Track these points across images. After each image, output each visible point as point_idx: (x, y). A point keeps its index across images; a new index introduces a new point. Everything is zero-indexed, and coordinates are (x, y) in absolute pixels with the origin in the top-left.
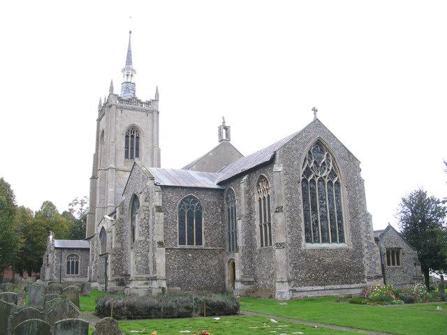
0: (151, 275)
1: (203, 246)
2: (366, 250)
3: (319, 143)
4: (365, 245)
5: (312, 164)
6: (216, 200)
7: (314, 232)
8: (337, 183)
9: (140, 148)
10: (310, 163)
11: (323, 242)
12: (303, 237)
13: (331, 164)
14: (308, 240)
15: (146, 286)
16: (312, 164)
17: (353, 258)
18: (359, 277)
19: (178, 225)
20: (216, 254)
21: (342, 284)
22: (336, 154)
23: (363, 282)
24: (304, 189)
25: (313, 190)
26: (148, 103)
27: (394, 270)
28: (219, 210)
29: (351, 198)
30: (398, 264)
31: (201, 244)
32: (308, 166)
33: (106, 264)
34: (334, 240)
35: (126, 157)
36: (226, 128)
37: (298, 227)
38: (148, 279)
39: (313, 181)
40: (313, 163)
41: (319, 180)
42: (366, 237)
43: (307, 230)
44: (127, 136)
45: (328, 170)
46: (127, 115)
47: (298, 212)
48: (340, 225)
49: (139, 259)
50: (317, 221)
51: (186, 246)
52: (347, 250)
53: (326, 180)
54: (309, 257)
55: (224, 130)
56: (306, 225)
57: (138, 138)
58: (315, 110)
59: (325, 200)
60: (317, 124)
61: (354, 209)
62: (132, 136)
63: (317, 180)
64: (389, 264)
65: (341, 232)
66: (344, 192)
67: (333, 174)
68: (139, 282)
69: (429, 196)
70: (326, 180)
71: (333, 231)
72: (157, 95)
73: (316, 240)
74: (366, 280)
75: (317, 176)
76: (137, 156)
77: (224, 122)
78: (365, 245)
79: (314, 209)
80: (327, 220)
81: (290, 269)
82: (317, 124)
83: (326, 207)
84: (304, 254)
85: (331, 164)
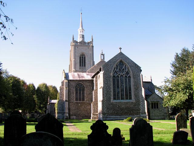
0: (64, 112)
2: (141, 103)
3: (121, 61)
4: (141, 100)
6: (90, 84)
7: (118, 95)
8: (130, 77)
9: (86, 62)
10: (117, 69)
12: (112, 98)
13: (127, 69)
14: (114, 99)
17: (135, 105)
18: (137, 113)
19: (75, 94)
21: (129, 115)
22: (128, 66)
23: (139, 115)
24: (113, 79)
25: (118, 81)
26: (89, 43)
27: (154, 111)
28: (92, 88)
29: (135, 82)
30: (157, 108)
31: (84, 101)
33: (69, 109)
34: (127, 99)
35: (80, 66)
37: (110, 94)
38: (63, 113)
39: (118, 76)
40: (118, 70)
41: (121, 76)
43: (114, 95)
44: (80, 57)
45: (125, 72)
46: (80, 49)
47: (110, 88)
48: (130, 93)
50: (119, 92)
51: (78, 101)
52: (132, 103)
53: (124, 76)
54: (115, 105)
55: (102, 56)
57: (85, 58)
58: (120, 49)
59: (123, 83)
60: (121, 54)
61: (136, 86)
62: (82, 57)
63: (119, 76)
64: (152, 108)
65: (130, 95)
66: (132, 79)
67: (127, 73)
68: (60, 114)
69: (48, 85)
70: (124, 76)
72: (92, 40)
73: (118, 99)
74: (141, 114)
75: (120, 74)
76: (85, 66)
77: (102, 53)
78: (141, 100)
79: (118, 87)
80: (124, 91)
82: (121, 54)
84: (112, 104)
85: (127, 69)
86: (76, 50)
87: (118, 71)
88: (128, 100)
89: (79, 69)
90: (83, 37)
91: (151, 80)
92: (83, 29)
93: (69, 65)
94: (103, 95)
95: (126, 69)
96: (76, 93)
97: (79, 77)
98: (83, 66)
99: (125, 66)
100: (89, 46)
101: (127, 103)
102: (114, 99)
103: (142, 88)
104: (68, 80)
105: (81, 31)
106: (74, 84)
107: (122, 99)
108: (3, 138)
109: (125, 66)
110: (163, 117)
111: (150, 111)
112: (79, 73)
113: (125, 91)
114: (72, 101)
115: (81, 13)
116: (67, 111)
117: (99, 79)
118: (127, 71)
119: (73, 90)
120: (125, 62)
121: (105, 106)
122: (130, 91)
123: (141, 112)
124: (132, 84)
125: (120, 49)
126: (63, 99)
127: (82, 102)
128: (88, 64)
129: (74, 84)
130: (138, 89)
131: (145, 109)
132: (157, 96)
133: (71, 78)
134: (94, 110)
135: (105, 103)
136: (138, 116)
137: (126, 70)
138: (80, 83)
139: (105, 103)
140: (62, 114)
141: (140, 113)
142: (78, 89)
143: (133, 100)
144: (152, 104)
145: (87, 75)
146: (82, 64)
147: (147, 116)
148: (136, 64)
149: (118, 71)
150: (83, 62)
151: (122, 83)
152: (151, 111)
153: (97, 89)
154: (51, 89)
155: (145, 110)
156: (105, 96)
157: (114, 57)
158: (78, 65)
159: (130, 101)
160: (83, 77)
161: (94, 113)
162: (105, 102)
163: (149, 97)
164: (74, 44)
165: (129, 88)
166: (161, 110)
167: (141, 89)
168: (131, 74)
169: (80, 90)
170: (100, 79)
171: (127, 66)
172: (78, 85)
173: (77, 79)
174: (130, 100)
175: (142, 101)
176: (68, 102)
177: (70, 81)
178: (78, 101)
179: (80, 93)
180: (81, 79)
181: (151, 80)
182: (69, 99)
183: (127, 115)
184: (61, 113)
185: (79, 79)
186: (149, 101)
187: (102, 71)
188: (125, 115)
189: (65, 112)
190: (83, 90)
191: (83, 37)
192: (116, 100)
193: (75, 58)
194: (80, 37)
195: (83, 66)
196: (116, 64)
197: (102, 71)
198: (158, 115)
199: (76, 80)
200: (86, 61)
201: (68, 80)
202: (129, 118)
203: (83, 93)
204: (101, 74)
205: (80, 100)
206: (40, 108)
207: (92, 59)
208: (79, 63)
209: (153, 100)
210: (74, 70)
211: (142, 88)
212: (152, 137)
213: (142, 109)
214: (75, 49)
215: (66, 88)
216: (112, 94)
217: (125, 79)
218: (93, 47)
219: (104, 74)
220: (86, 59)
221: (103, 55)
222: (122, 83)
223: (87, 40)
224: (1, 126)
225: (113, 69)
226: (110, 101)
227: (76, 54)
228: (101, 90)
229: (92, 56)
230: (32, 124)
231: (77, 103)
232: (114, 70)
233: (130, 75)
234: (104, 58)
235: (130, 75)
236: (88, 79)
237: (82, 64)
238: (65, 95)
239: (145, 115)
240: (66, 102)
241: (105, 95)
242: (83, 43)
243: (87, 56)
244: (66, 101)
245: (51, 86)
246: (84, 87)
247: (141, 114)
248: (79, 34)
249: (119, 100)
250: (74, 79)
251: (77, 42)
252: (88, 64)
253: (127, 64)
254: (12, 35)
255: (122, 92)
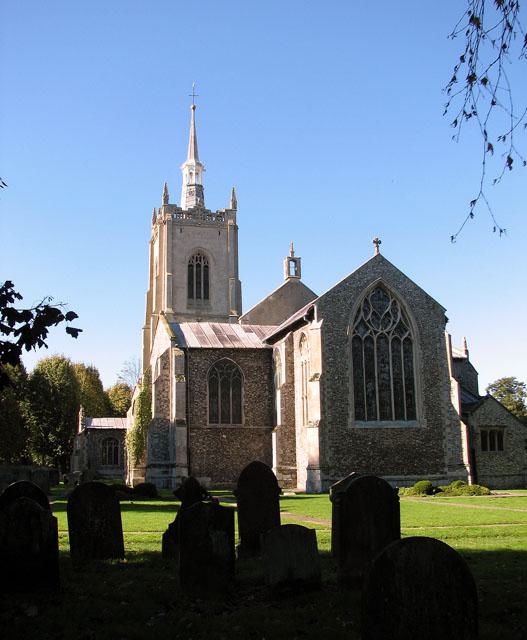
0: (171, 462)
1: (242, 425)
2: (448, 430)
3: (380, 287)
5: (370, 316)
6: (260, 363)
7: (369, 405)
8: (408, 341)
10: (366, 314)
11: (382, 419)
12: (351, 413)
13: (399, 314)
14: (359, 417)
15: (166, 475)
16: (370, 316)
19: (208, 397)
20: (260, 435)
21: (408, 474)
23: (442, 473)
24: (354, 349)
25: (370, 359)
26: (220, 215)
27: (491, 458)
28: (266, 377)
29: (427, 360)
30: (501, 448)
32: (362, 320)
34: (399, 417)
35: (190, 296)
36: (294, 260)
37: (344, 401)
38: (167, 466)
40: (370, 316)
42: (448, 411)
43: (358, 404)
44: (190, 266)
45: (394, 323)
48: (411, 397)
49: (156, 441)
50: (374, 392)
51: (219, 425)
52: (418, 430)
54: (359, 438)
55: (292, 264)
56: (356, 396)
57: (206, 267)
58: (377, 242)
59: (388, 363)
60: (379, 260)
62: (199, 266)
64: (484, 448)
65: (412, 405)
66: (416, 350)
68: (157, 470)
71: (398, 404)
73: (372, 416)
75: (376, 332)
76: (207, 297)
77: (293, 253)
78: (447, 422)
79: (370, 375)
81: (330, 454)
82: (379, 260)
83: (389, 373)
84: (352, 434)
85: (399, 314)
86: (176, 241)
87: (369, 321)
88: (403, 422)
89: (188, 308)
90: (199, 191)
91: (467, 352)
92: (200, 165)
93: (150, 294)
94: (323, 402)
95: (395, 314)
96: (213, 395)
97: (222, 339)
98: (199, 297)
99: (394, 303)
100: (224, 226)
101: (401, 431)
102: (359, 417)
103: (451, 378)
104: (185, 349)
105: (194, 172)
106: (204, 364)
107: (384, 417)
108: (68, 556)
109: (394, 303)
110: (518, 480)
111: (477, 459)
112: (216, 324)
113: (395, 389)
114: (197, 424)
115: (194, 108)
116: (182, 459)
117: (300, 346)
118: (400, 322)
119: (203, 386)
120: (393, 291)
121: (329, 443)
122: (411, 392)
123: (447, 462)
124: (417, 364)
125: (377, 242)
126: (168, 418)
127: (230, 426)
128: (220, 289)
129: (204, 364)
130: (438, 385)
131: (461, 450)
132: (498, 407)
133: (193, 342)
134: (281, 456)
135: (327, 430)
136: (438, 475)
137: (396, 317)
138: (226, 361)
139: (327, 430)
140: (165, 470)
141: (444, 465)
142: (220, 380)
143: (421, 421)
144: (484, 434)
145: (248, 331)
146: (199, 287)
147: (470, 478)
148: (429, 299)
149: (369, 321)
150: (199, 283)
151: (384, 362)
152: (481, 457)
153: (293, 382)
154: (82, 379)
155: (461, 456)
156: (326, 408)
157: (358, 271)
158: (183, 293)
159: (404, 424)
160: (233, 338)
161: (283, 467)
162: (330, 427)
163: (472, 412)
164: (169, 217)
165: (406, 379)
166: (511, 454)
167: (449, 382)
168: (413, 331)
169: (225, 385)
170: (304, 344)
171: (400, 301)
172: (217, 365)
173: (216, 346)
174: (410, 422)
175: (450, 425)
176: (185, 429)
177: (189, 353)
178: (219, 425)
179: (225, 395)
180: (229, 345)
181: (467, 352)
182: (187, 417)
183: (403, 473)
184: (160, 466)
185: (222, 347)
186: (474, 424)
187: (315, 321)
188: (395, 475)
189: (177, 461)
190: (238, 385)
191: (199, 191)
192: (362, 422)
193: (171, 268)
194: (191, 193)
195: (199, 297)
196: (362, 296)
197: (318, 321)
198: (504, 473)
199: (209, 349)
200: (213, 280)
201: (185, 349)
202: (424, 483)
203: (237, 396)
204: (313, 331)
205: (225, 420)
206: (45, 448)
207: (232, 273)
208: (186, 287)
209: (488, 421)
210: (170, 310)
211: (451, 378)
212: (57, 547)
213: (449, 453)
214: (172, 235)
215: (178, 376)
216: (351, 398)
217: (393, 347)
218: (236, 228)
219: (325, 331)
220: (212, 271)
221: (296, 261)
222: (384, 362)
223: (214, 204)
224: (515, 544)
225: (355, 313)
226: (346, 425)
227: (175, 253)
228: (315, 389)
229: (232, 261)
230: (144, 505)
231: (216, 431)
232: (357, 317)
233: (409, 335)
234: (298, 273)
235: (409, 335)
236: (253, 346)
237: (199, 287)
238: (173, 401)
239: (460, 473)
240: (181, 428)
241: (329, 403)
242: (199, 213)
243: (214, 260)
244: (179, 422)
245: (82, 368)
246: (240, 375)
247: (446, 469)
248: (185, 183)
249: (373, 422)
250: (206, 346)
251: (179, 211)
252: (220, 289)
253: (400, 297)
254: (498, 231)
255: (384, 394)
